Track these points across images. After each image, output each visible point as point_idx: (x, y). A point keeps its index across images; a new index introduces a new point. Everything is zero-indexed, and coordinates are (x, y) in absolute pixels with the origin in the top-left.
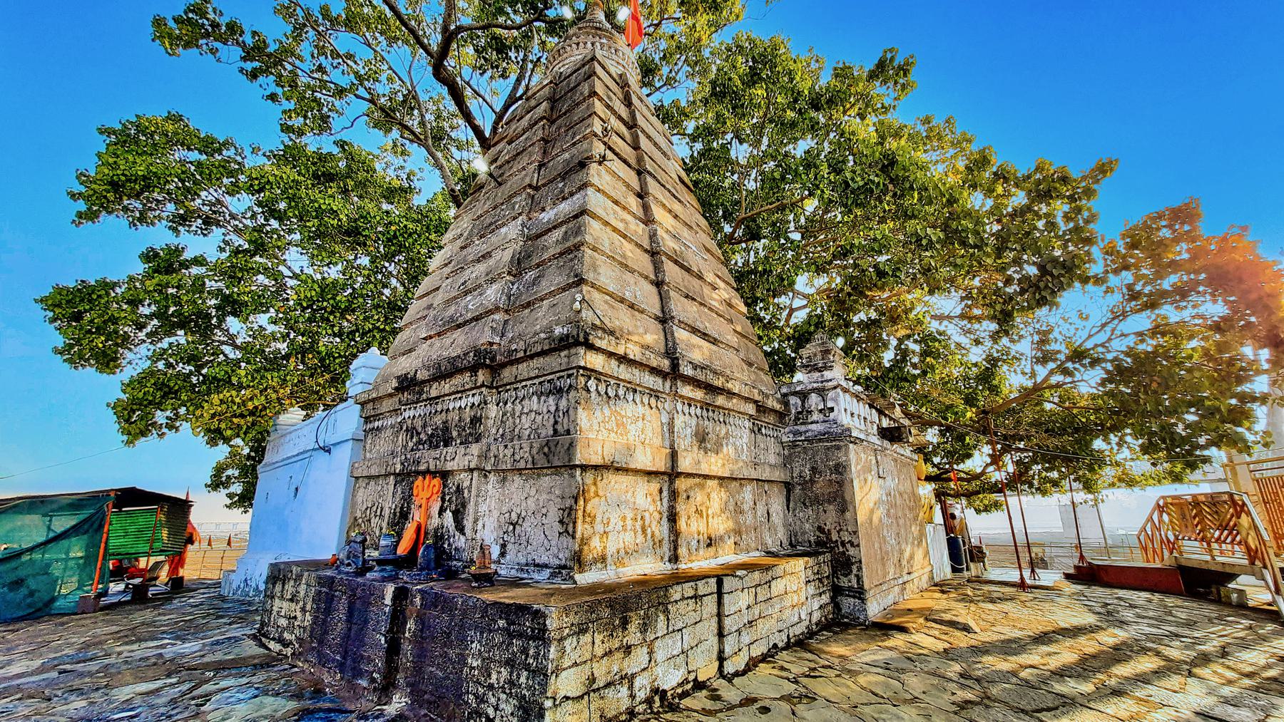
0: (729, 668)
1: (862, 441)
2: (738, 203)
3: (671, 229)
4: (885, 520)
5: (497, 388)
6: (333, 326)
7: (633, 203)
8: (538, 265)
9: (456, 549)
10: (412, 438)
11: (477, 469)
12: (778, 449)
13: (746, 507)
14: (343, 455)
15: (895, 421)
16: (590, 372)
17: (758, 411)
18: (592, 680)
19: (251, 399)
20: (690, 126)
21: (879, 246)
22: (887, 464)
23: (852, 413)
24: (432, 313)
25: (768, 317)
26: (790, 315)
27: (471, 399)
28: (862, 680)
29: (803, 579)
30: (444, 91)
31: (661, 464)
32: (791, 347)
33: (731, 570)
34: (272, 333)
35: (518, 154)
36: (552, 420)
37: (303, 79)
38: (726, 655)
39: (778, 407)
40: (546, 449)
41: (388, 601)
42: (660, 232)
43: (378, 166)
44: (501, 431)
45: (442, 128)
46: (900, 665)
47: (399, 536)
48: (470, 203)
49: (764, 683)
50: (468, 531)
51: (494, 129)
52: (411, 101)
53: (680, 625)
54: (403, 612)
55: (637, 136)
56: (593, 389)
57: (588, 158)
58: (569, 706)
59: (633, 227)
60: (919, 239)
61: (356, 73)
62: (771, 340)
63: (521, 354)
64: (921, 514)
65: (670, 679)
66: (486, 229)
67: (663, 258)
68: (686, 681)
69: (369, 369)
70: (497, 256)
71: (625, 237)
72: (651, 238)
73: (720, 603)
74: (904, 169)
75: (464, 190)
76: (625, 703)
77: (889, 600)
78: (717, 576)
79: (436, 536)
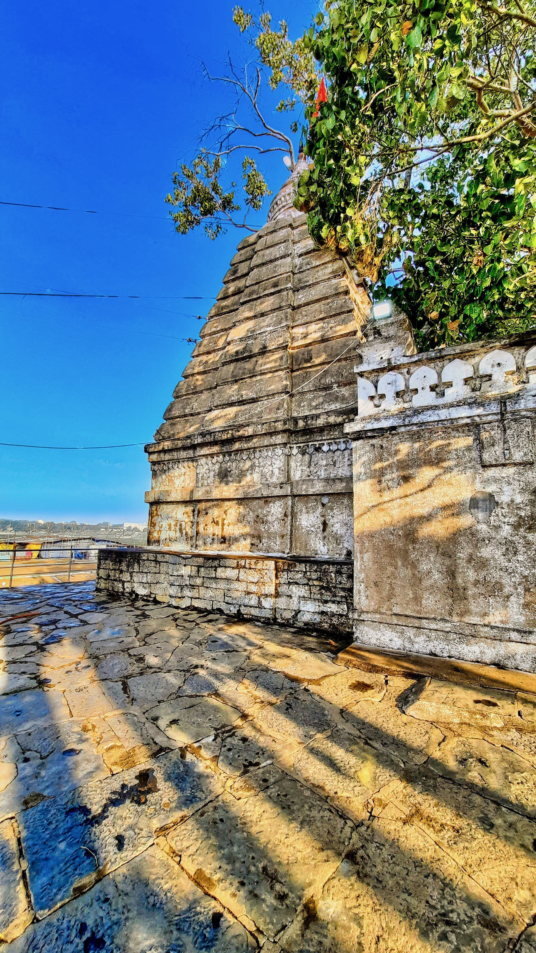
28: (523, 775)
53: (146, 571)
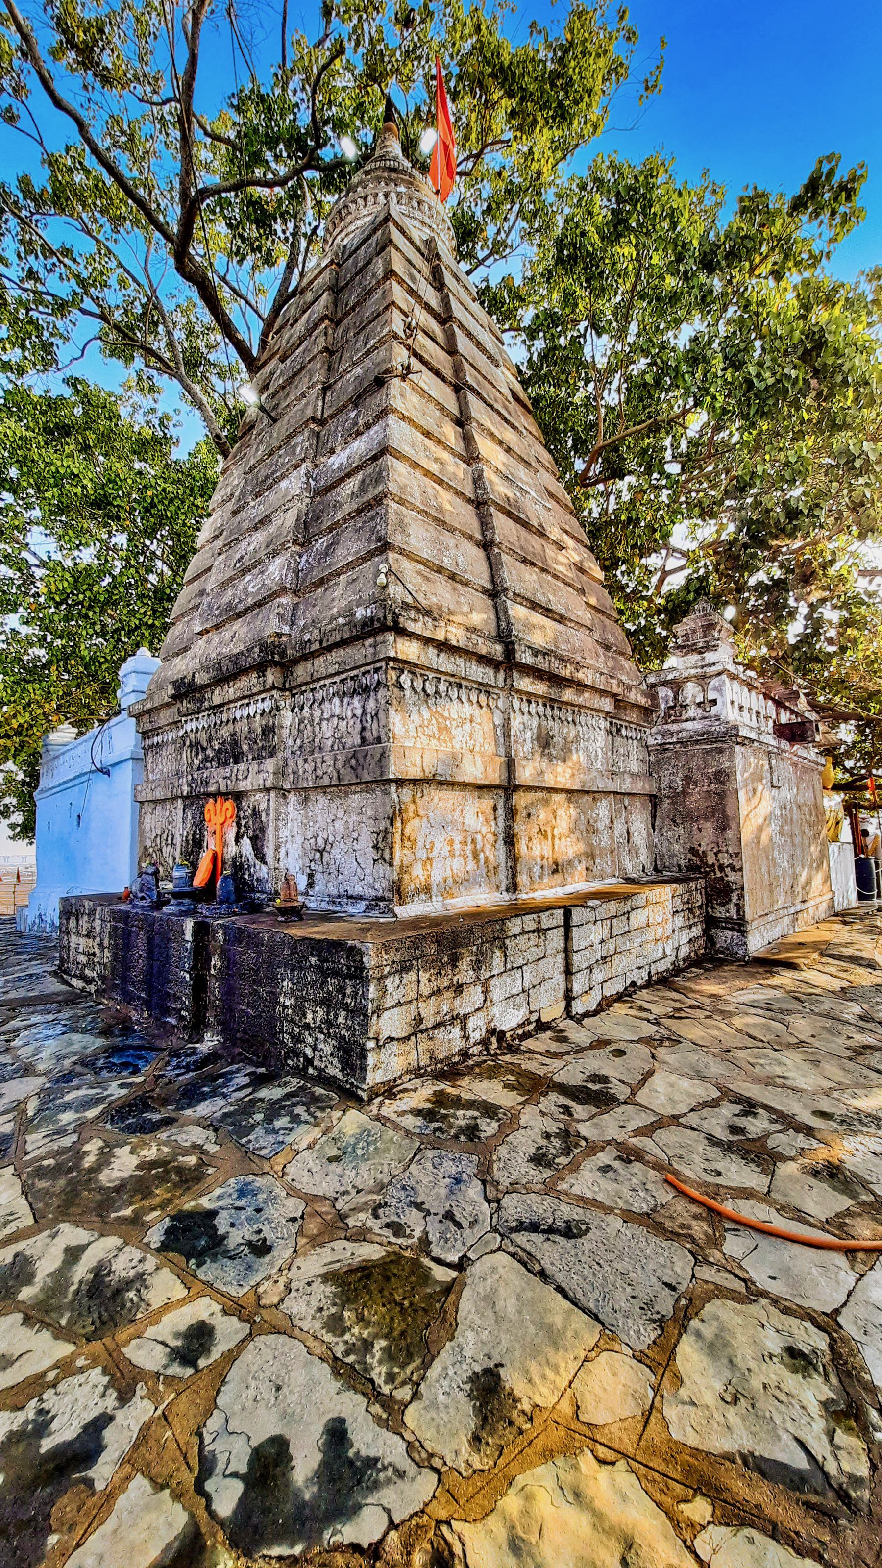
0: (578, 1007)
1: (753, 741)
2: (593, 426)
3: (501, 468)
4: (777, 839)
5: (290, 690)
6: (94, 624)
7: (450, 433)
8: (330, 529)
9: (258, 880)
10: (197, 754)
11: (274, 788)
12: (643, 754)
13: (600, 826)
14: (125, 777)
15: (797, 715)
16: (402, 665)
17: (617, 707)
18: (419, 1020)
19: (15, 716)
20: (527, 315)
21: (792, 473)
22: (784, 770)
23: (741, 705)
24: (206, 600)
25: (632, 584)
26: (661, 581)
27: (260, 706)
28: (738, 1022)
29: (670, 909)
30: (194, 293)
31: (495, 776)
32: (662, 622)
33: (582, 900)
34: (27, 636)
35: (295, 375)
36: (358, 727)
37: (12, 292)
38: (575, 994)
39: (643, 701)
40: (353, 762)
41: (188, 936)
42: (489, 474)
43: (123, 411)
44: (299, 742)
45: (196, 349)
46: (784, 1006)
47: (194, 866)
48: (239, 450)
49: (619, 1024)
50: (269, 858)
51: (263, 343)
52: (152, 313)
53: (521, 962)
54: (206, 947)
55: (453, 334)
56: (407, 685)
57: (387, 371)
58: (394, 1047)
59: (451, 469)
60: (851, 459)
61: (77, 276)
62: (636, 615)
63: (317, 646)
64: (824, 832)
65: (509, 1019)
66: (262, 486)
67: (492, 509)
68: (528, 1022)
69: (141, 673)
70: (277, 521)
71: (440, 482)
72: (475, 481)
73: (567, 937)
74: (837, 353)
75: (232, 433)
76: (458, 1044)
77: (775, 933)
78: (564, 907)
79: (234, 865)
